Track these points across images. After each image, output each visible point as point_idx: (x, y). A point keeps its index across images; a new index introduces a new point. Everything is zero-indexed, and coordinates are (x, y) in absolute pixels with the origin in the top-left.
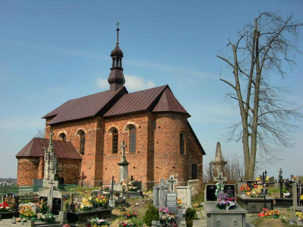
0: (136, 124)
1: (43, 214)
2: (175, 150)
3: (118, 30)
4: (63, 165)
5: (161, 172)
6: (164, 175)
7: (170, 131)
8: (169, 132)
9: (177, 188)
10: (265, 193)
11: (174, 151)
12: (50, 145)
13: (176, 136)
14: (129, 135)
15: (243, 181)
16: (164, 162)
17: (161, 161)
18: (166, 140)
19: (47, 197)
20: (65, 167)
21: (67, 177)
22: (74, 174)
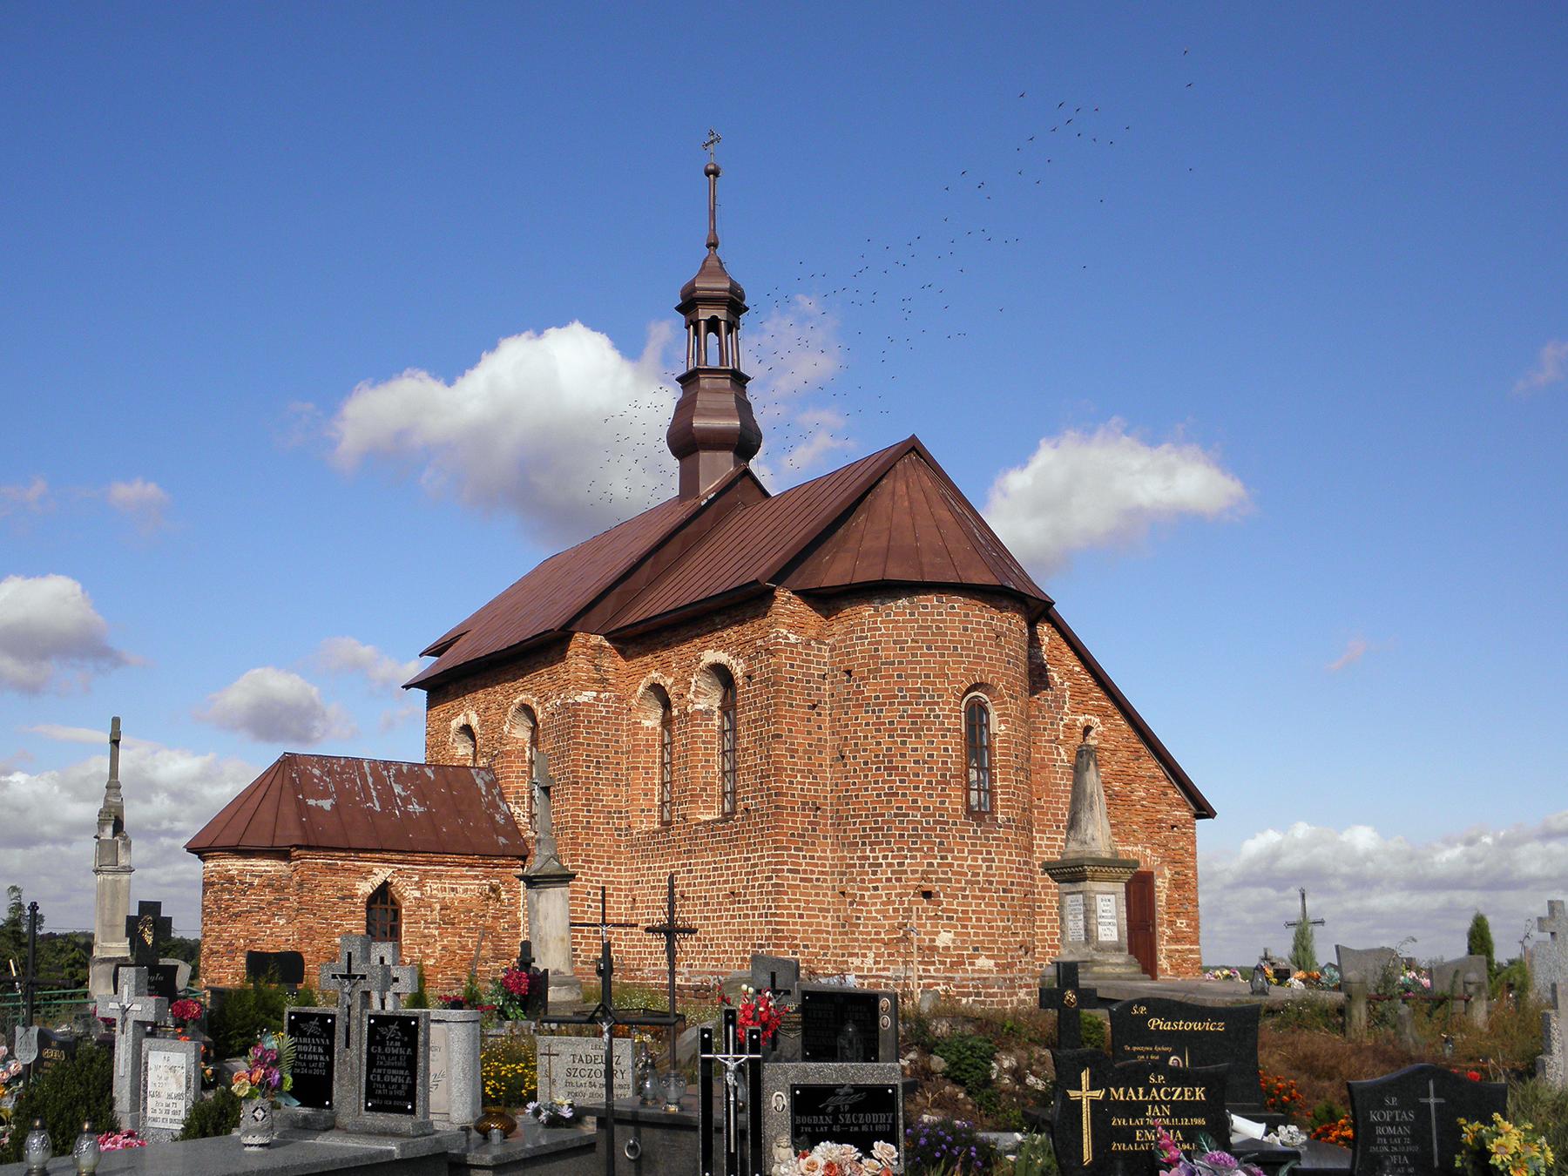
0: (734, 663)
2: (930, 796)
3: (713, 245)
4: (420, 885)
6: (877, 933)
7: (901, 690)
8: (896, 697)
13: (937, 716)
14: (717, 722)
16: (871, 865)
18: (879, 744)
19: (794, 1088)
20: (431, 897)
21: (444, 948)
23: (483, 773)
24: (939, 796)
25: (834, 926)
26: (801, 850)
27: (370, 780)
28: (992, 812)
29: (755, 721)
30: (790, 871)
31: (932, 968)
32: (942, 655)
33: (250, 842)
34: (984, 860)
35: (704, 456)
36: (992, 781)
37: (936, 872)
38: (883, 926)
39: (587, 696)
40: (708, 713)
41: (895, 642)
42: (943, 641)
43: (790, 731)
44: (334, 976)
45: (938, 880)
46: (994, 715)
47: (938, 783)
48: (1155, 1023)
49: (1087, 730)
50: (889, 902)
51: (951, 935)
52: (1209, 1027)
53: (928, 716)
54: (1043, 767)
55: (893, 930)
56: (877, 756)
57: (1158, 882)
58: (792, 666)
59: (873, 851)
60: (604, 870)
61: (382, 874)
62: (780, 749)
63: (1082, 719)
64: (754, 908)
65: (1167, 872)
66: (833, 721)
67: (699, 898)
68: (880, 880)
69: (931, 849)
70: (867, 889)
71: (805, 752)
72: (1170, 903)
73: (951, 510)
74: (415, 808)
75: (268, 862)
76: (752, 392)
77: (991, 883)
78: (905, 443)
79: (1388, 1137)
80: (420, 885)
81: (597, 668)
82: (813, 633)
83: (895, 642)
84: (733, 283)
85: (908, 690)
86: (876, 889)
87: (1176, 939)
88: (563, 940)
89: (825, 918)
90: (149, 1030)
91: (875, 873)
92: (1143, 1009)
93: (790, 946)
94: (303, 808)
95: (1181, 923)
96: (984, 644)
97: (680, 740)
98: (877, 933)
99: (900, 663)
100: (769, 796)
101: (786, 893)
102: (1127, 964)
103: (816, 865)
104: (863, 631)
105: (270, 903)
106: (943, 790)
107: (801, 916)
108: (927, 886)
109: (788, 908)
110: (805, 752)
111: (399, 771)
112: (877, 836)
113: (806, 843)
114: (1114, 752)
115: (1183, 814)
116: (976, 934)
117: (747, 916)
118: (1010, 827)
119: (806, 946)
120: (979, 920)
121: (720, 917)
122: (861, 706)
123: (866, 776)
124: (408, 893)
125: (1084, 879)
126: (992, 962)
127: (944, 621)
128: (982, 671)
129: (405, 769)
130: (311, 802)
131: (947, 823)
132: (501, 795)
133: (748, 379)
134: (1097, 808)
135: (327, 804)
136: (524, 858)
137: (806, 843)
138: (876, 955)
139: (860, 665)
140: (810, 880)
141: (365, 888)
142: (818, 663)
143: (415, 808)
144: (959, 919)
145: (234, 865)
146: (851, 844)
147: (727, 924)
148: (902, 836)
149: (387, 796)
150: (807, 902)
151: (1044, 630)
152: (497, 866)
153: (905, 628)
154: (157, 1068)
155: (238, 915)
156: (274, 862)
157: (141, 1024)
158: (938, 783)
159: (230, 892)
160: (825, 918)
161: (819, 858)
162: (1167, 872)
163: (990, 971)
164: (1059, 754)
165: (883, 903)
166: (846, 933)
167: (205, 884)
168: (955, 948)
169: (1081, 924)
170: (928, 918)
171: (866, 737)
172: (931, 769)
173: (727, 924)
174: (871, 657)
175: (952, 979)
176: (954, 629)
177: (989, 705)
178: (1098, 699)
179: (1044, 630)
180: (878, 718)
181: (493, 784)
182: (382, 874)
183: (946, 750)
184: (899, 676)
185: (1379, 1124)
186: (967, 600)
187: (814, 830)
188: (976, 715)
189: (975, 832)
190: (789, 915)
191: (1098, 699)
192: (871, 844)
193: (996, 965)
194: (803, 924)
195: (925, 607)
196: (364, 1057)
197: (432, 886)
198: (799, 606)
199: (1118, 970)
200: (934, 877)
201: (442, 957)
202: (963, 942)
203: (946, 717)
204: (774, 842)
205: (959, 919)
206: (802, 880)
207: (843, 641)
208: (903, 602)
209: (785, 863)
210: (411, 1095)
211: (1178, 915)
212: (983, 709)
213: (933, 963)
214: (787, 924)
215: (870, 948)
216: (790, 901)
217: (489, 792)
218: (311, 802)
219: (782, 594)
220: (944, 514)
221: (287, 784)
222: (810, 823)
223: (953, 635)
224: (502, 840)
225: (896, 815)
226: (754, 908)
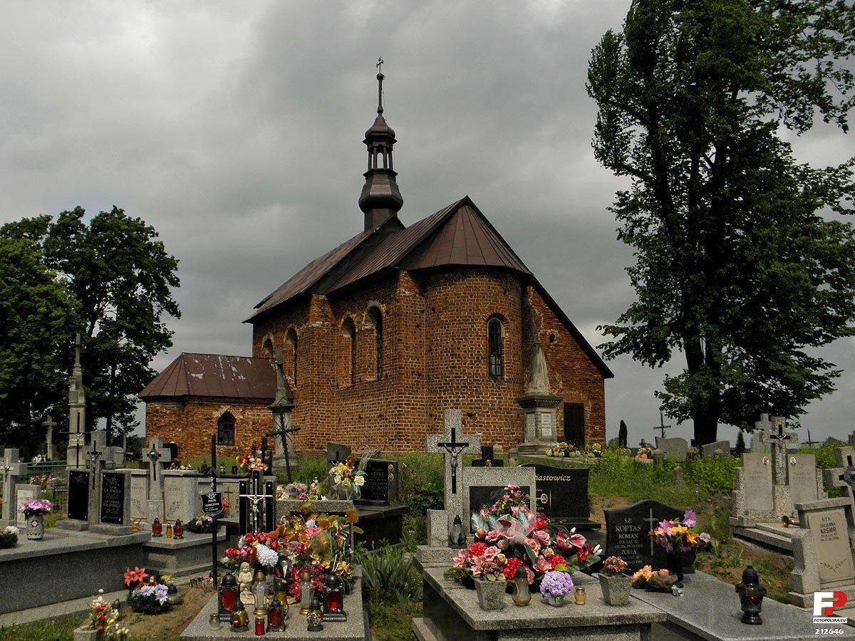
1: (441, 506)
2: (472, 368)
3: (380, 78)
4: (243, 413)
5: (438, 426)
8: (455, 320)
9: (166, 476)
10: (215, 507)
11: (470, 370)
12: (23, 357)
14: (375, 335)
15: (97, 453)
17: (438, 398)
18: (447, 343)
20: (248, 418)
25: (427, 430)
26: (411, 394)
28: (502, 375)
30: (405, 404)
34: (497, 398)
35: (375, 212)
36: (502, 361)
39: (318, 324)
40: (371, 330)
43: (406, 337)
44: (88, 453)
45: (475, 408)
46: (503, 329)
53: (471, 329)
57: (586, 408)
59: (444, 394)
61: (224, 409)
64: (390, 422)
66: (426, 333)
67: (367, 418)
74: (241, 377)
77: (501, 409)
78: (462, 201)
79: (625, 540)
80: (243, 413)
89: (423, 426)
90: (18, 480)
91: (445, 405)
94: (188, 377)
95: (597, 428)
97: (359, 343)
100: (396, 369)
103: (419, 401)
105: (174, 422)
107: (411, 426)
113: (414, 391)
116: (494, 433)
117: (386, 426)
118: (511, 382)
119: (413, 440)
120: (495, 426)
121: (375, 427)
123: (441, 359)
124: (238, 417)
126: (501, 447)
127: (479, 284)
130: (194, 375)
135: (200, 376)
137: (414, 391)
141: (217, 414)
143: (241, 377)
146: (435, 391)
147: (378, 430)
151: (531, 289)
154: (21, 498)
157: (13, 477)
159: (157, 416)
160: (423, 426)
161: (420, 398)
163: (500, 451)
167: (147, 413)
169: (534, 428)
170: (470, 426)
172: (472, 355)
173: (378, 430)
180: (447, 330)
182: (224, 409)
185: (620, 533)
190: (405, 425)
193: (503, 448)
196: (101, 493)
197: (248, 413)
200: (473, 406)
202: (487, 437)
203: (479, 329)
204: (398, 390)
210: (121, 514)
211: (595, 423)
214: (404, 429)
218: (194, 375)
226: (390, 422)
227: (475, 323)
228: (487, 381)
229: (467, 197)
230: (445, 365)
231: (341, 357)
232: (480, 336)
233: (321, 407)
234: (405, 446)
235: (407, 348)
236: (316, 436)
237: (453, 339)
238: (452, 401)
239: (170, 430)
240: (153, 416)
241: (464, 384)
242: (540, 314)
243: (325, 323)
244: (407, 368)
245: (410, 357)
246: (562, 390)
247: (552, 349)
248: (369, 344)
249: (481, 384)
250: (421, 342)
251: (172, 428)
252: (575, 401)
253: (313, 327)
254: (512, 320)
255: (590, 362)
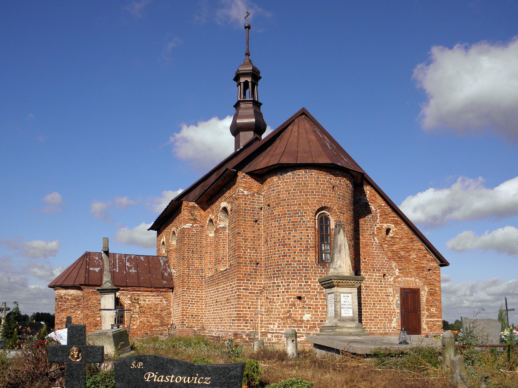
3: (248, 54)
5: (272, 308)
8: (286, 214)
13: (304, 222)
16: (276, 286)
18: (279, 234)
21: (140, 322)
22: (158, 316)
23: (164, 258)
24: (304, 256)
26: (249, 280)
27: (117, 261)
29: (233, 228)
30: (244, 289)
31: (301, 329)
32: (307, 195)
33: (66, 283)
35: (241, 133)
37: (303, 289)
38: (281, 312)
39: (188, 226)
40: (224, 228)
41: (286, 191)
42: (307, 189)
43: (244, 231)
45: (304, 292)
47: (304, 250)
48: (151, 376)
49: (388, 231)
50: (283, 301)
51: (310, 315)
52: (196, 380)
53: (300, 222)
54: (367, 245)
55: (285, 313)
56: (279, 240)
57: (422, 293)
58: (245, 204)
59: (277, 280)
60: (195, 292)
62: (239, 239)
63: (385, 226)
65: (426, 289)
66: (264, 227)
68: (280, 292)
69: (301, 279)
70: (275, 296)
71: (252, 240)
72: (427, 301)
73: (317, 136)
74: (133, 271)
75: (74, 291)
76: (263, 109)
81: (192, 215)
82: (255, 190)
83: (286, 191)
84: (254, 67)
85: (292, 211)
86: (278, 296)
87: (431, 316)
88: (113, 317)
91: (278, 289)
92: (141, 364)
93: (244, 320)
94: (88, 271)
95: (433, 310)
96: (327, 190)
98: (279, 315)
99: (288, 199)
101: (242, 298)
102: (356, 328)
103: (257, 287)
104: (274, 187)
105: (74, 306)
106: (307, 253)
107: (249, 308)
108: (299, 295)
109: (244, 304)
110: (252, 240)
111: (130, 258)
112: (279, 274)
113: (252, 278)
114: (401, 239)
115: (434, 264)
119: (251, 320)
122: (273, 219)
123: (275, 249)
125: (334, 286)
127: (308, 181)
128: (326, 202)
129: (133, 257)
130: (91, 269)
131: (308, 267)
132: (169, 266)
133: (261, 104)
134: (343, 252)
136: (173, 289)
137: (252, 278)
138: (279, 324)
139: (273, 202)
140: (254, 293)
142: (258, 203)
144: (313, 308)
145: (63, 292)
148: (289, 273)
149: (123, 266)
150: (252, 302)
152: (162, 292)
153: (290, 185)
155: (64, 310)
156: (76, 291)
158: (304, 250)
159: (61, 302)
161: (258, 284)
162: (426, 289)
164: (374, 240)
165: (281, 302)
166: (268, 315)
168: (312, 321)
169: (333, 308)
170: (300, 308)
171: (275, 232)
174: (277, 198)
175: (309, 334)
176: (312, 184)
177: (330, 217)
178: (393, 217)
179: (367, 189)
180: (280, 223)
181: (166, 262)
183: (308, 236)
184: (288, 205)
186: (318, 171)
187: (256, 272)
188: (324, 221)
189: (322, 271)
190: (243, 308)
191: (393, 217)
192: (277, 277)
194: (250, 311)
195: (299, 175)
198: (249, 180)
199: (351, 330)
201: (140, 325)
203: (307, 221)
204: (238, 277)
205: (313, 308)
206: (250, 293)
207: (267, 192)
208: (290, 173)
209: (242, 286)
211: (431, 306)
212: (327, 219)
213: (302, 327)
214: (243, 311)
215: (276, 321)
216: (244, 301)
217: (164, 265)
218: (91, 269)
219: (241, 174)
220: (313, 137)
221: (84, 263)
222: (253, 269)
223: (312, 186)
224: (165, 282)
225: (286, 265)
227: (304, 216)
228: (315, 267)
229: (304, 109)
230: (277, 254)
231: (207, 253)
232: (309, 227)
233: (191, 294)
234: (244, 326)
235: (246, 240)
236: (187, 318)
237: (284, 231)
238: (284, 286)
239: (71, 312)
240: (59, 301)
241: (294, 270)
242: (376, 211)
243: (194, 225)
244: (246, 258)
245: (248, 248)
246: (398, 277)
247: (389, 241)
248: (223, 240)
249: (310, 270)
250: (259, 235)
251: (73, 311)
252: (412, 286)
253: (184, 228)
254: (341, 213)
255: (425, 252)
